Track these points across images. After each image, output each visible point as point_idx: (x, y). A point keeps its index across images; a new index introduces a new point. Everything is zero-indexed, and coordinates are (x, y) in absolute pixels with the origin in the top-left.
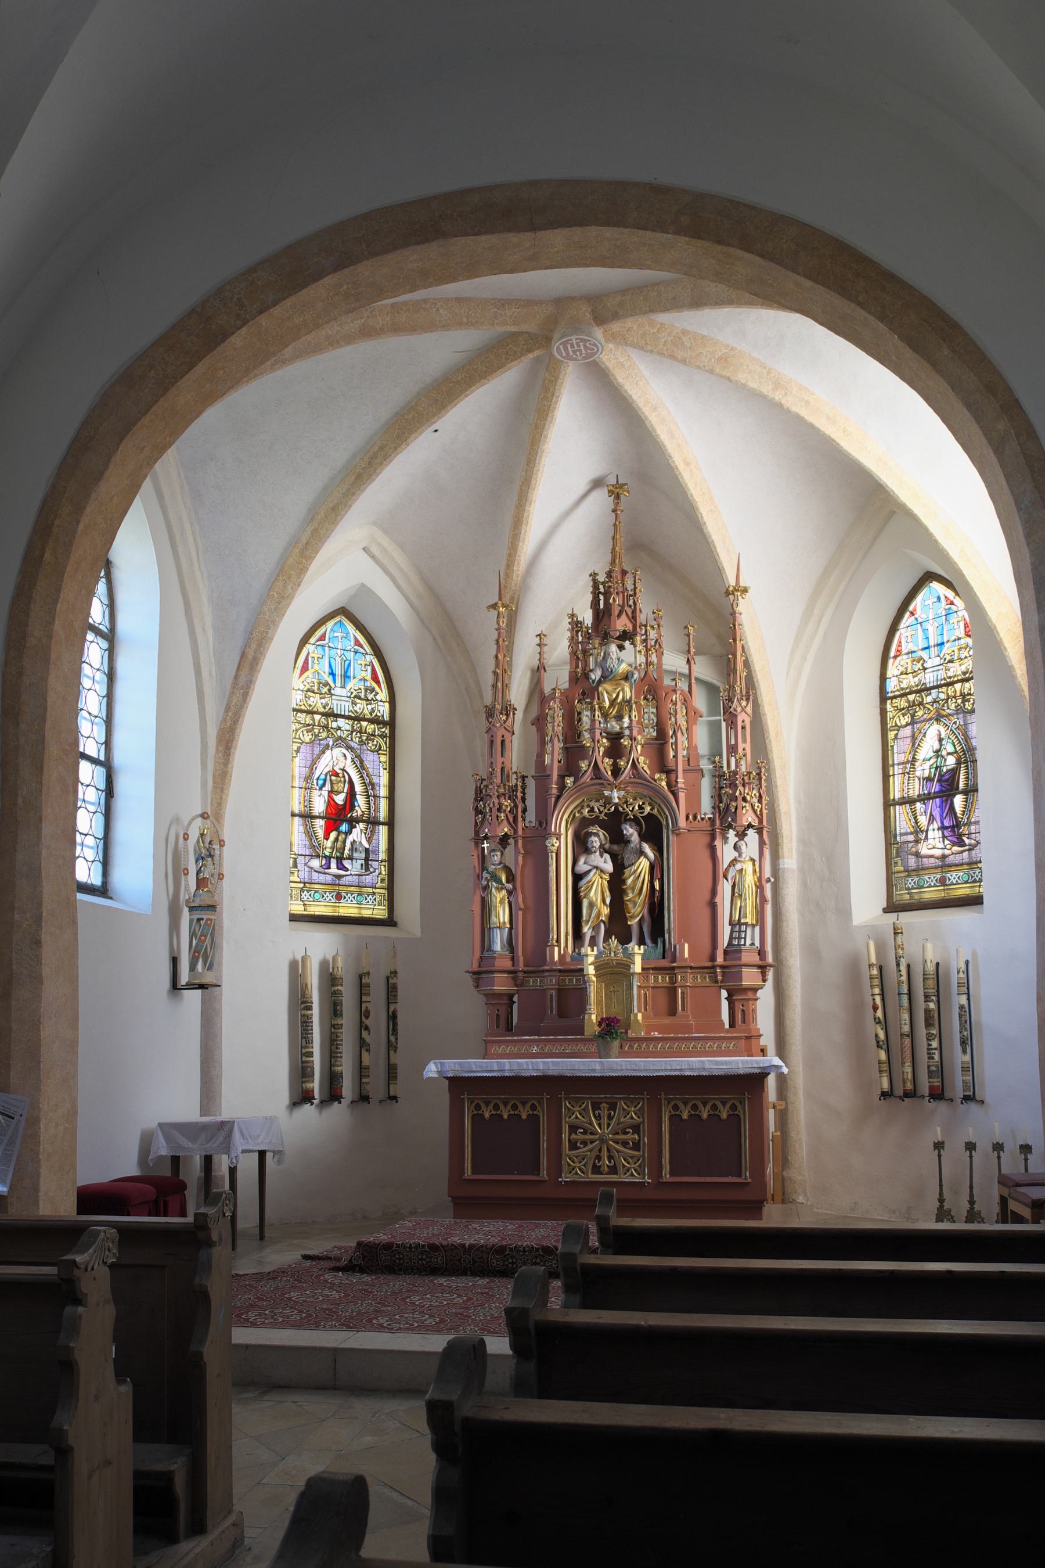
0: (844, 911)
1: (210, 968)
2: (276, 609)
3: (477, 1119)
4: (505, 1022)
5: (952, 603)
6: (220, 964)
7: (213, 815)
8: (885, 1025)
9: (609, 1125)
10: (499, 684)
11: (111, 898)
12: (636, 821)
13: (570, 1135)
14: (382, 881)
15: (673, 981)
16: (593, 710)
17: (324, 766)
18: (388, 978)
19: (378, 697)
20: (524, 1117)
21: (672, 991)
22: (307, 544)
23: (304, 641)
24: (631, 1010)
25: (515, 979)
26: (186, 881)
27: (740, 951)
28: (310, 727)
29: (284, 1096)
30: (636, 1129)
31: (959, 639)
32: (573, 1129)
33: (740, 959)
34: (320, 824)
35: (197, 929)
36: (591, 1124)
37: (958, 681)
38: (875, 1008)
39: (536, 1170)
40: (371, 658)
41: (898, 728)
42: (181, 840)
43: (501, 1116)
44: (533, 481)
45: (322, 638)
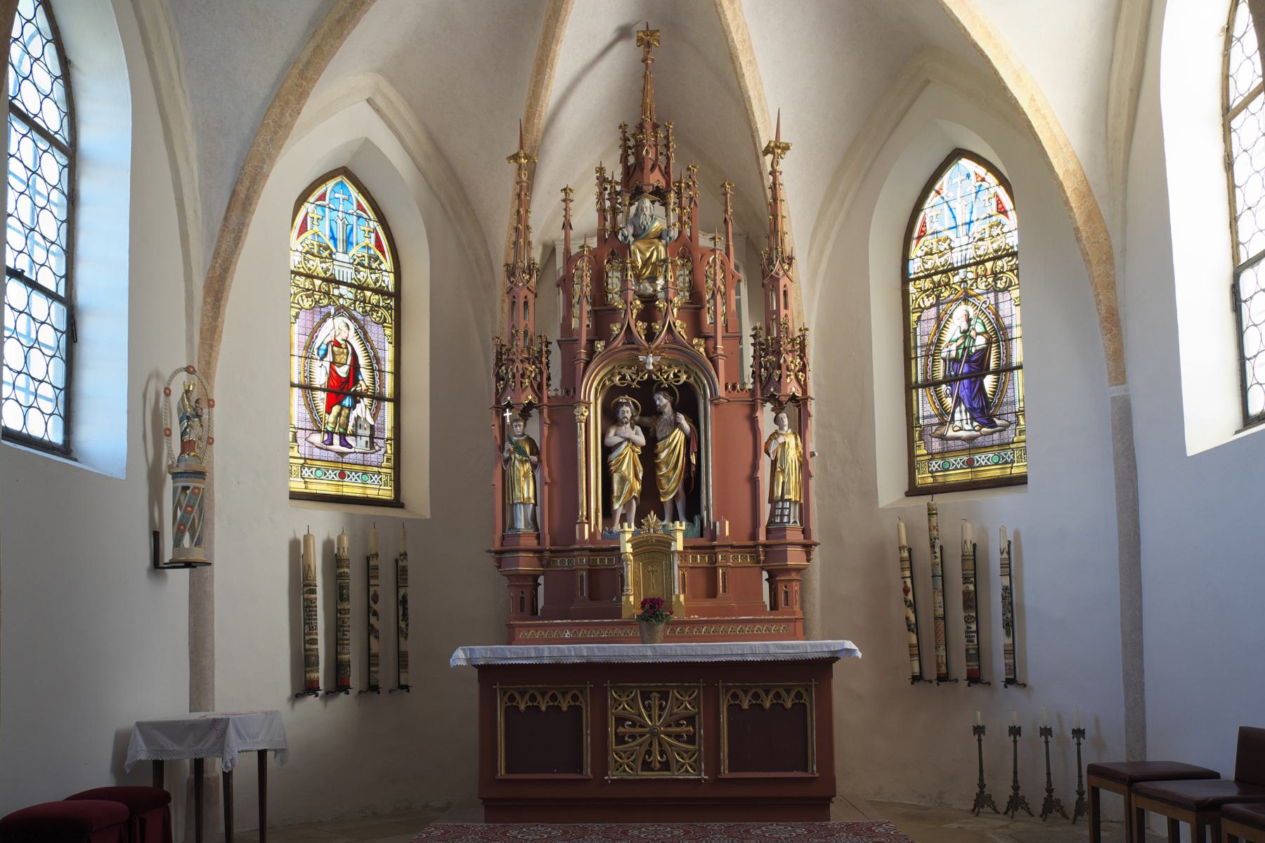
0: (869, 494)
1: (198, 544)
2: (272, 140)
3: (511, 711)
4: (525, 608)
5: (983, 180)
6: (211, 542)
7: (201, 369)
8: (913, 606)
9: (660, 716)
10: (521, 240)
11: (76, 460)
12: (669, 391)
13: (616, 728)
14: (388, 460)
15: (713, 560)
16: (624, 270)
17: (327, 332)
18: (397, 561)
19: (383, 267)
20: (565, 708)
21: (711, 572)
22: (308, 63)
23: (302, 199)
24: (670, 591)
25: (540, 559)
26: (170, 448)
27: (784, 529)
28: (309, 293)
29: (286, 689)
30: (691, 720)
31: (990, 216)
32: (620, 721)
33: (785, 537)
34: (321, 397)
35: (182, 498)
36: (640, 715)
37: (989, 260)
38: (906, 591)
39: (579, 767)
40: (373, 224)
41: (922, 310)
42: (162, 395)
43: (538, 708)
44: (563, 12)
45: (322, 197)
